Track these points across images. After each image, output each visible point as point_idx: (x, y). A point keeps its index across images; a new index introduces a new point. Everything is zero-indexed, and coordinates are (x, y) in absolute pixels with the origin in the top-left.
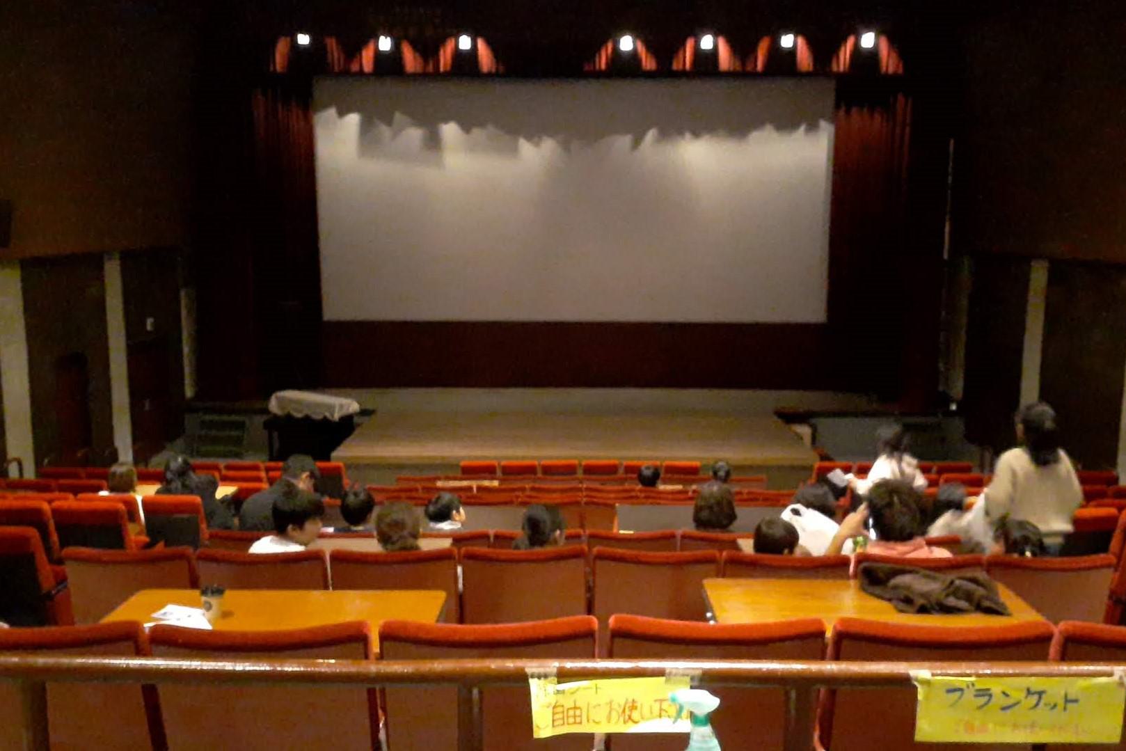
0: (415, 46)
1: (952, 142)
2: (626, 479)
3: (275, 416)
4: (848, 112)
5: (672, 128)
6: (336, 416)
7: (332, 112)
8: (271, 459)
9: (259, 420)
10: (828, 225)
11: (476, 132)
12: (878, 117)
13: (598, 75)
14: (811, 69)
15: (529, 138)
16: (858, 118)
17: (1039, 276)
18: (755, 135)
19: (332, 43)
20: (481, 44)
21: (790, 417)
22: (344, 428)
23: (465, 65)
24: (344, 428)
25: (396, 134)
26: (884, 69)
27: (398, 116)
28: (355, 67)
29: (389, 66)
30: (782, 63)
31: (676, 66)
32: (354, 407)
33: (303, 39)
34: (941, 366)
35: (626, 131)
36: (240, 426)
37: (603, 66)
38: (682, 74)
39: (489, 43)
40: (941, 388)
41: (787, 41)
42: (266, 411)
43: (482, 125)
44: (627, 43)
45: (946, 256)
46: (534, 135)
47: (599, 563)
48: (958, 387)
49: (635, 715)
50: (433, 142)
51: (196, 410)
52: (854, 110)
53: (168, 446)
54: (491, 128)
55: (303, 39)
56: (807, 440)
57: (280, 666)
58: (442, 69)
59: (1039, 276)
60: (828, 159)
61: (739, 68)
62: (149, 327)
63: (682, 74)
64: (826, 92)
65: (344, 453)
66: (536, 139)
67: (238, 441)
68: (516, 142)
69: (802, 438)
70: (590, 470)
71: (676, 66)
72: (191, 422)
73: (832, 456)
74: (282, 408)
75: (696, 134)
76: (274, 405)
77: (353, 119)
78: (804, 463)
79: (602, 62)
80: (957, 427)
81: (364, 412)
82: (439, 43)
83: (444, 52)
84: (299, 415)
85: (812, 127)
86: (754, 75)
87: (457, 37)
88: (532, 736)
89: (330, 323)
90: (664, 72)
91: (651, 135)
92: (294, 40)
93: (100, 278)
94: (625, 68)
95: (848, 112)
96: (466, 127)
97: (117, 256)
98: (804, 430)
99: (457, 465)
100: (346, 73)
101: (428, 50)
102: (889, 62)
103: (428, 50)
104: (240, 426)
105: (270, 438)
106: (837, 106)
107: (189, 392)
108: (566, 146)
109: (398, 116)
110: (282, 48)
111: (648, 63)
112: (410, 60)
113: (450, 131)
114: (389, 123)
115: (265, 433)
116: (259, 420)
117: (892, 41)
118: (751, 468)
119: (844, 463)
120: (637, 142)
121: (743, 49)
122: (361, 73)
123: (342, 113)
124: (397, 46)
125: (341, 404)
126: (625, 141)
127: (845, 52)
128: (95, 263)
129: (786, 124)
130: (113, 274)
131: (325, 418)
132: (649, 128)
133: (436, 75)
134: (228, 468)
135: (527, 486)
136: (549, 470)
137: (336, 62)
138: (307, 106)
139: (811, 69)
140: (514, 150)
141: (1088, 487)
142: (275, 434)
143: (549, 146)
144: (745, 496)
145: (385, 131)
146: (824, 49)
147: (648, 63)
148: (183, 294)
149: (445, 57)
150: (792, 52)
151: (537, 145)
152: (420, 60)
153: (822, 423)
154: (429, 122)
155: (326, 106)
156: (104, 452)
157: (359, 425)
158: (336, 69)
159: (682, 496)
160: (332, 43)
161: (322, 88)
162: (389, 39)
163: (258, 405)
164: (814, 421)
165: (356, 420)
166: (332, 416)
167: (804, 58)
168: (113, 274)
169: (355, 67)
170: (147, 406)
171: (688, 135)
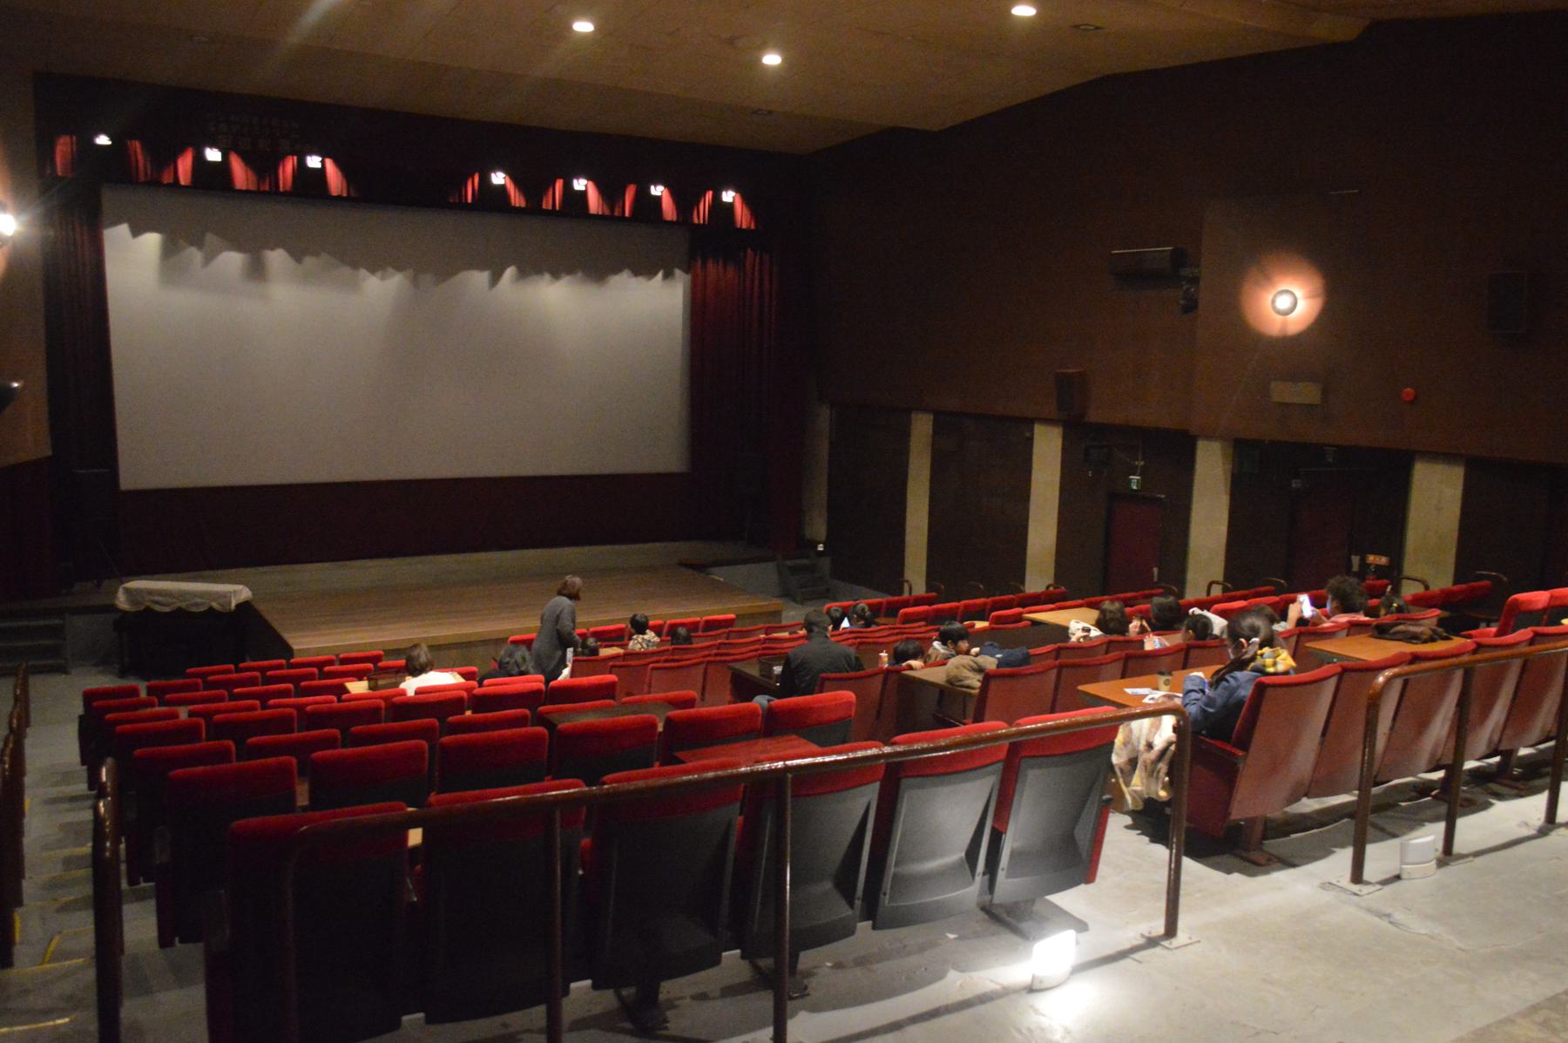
0: (248, 160)
3: (125, 613)
5: (530, 268)
7: (124, 229)
11: (309, 261)
12: (731, 269)
13: (462, 206)
14: (675, 219)
15: (373, 271)
17: (922, 428)
19: (136, 145)
20: (329, 163)
23: (212, 180)
25: (208, 259)
26: (513, 204)
27: (210, 238)
28: (167, 178)
31: (547, 204)
33: (103, 140)
35: (481, 267)
37: (469, 200)
38: (552, 213)
39: (337, 162)
41: (314, 162)
42: (112, 608)
43: (316, 254)
46: (376, 265)
49: (1269, 610)
50: (257, 270)
52: (710, 265)
54: (325, 257)
57: (593, 790)
58: (281, 189)
59: (922, 428)
60: (685, 306)
61: (607, 212)
71: (547, 204)
75: (556, 275)
77: (152, 241)
83: (284, 172)
84: (167, 609)
90: (533, 209)
91: (510, 272)
94: (494, 200)
96: (297, 255)
100: (154, 183)
102: (742, 217)
103: (263, 165)
108: (415, 281)
109: (210, 238)
111: (517, 199)
112: (241, 174)
113: (277, 258)
114: (198, 244)
119: (626, 638)
120: (496, 278)
121: (610, 193)
123: (136, 231)
126: (480, 278)
129: (644, 269)
133: (274, 193)
139: (675, 219)
141: (529, 723)
145: (195, 255)
146: (685, 202)
147: (517, 199)
150: (584, 194)
152: (253, 178)
154: (254, 248)
155: (116, 222)
158: (142, 179)
167: (594, 202)
171: (547, 276)
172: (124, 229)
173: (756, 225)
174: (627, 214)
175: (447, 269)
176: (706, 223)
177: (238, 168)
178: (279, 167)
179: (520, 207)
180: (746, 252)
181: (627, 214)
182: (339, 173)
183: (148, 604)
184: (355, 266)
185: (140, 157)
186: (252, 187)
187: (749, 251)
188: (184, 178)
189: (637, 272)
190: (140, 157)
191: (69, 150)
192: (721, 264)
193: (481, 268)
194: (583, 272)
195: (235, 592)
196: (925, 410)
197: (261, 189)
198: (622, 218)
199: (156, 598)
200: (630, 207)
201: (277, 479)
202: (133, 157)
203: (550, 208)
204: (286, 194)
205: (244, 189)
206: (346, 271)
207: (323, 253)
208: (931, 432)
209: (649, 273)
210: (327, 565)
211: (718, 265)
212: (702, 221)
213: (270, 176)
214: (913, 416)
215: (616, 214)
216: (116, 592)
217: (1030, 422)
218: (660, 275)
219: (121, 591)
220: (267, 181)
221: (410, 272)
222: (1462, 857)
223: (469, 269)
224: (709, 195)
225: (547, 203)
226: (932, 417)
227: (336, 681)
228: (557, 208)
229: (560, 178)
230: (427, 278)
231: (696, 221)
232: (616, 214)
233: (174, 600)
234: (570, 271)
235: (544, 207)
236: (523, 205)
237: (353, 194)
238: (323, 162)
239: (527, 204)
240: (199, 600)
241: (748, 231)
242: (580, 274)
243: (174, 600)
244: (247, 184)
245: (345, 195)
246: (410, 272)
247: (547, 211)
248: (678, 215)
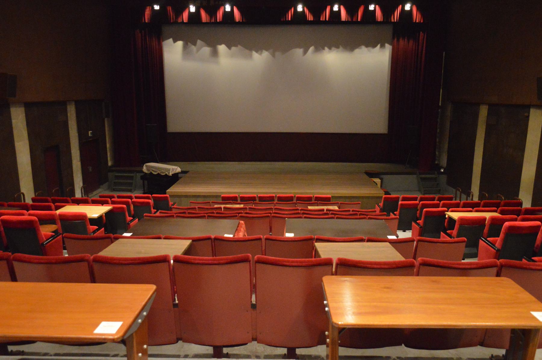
0: (206, 11)
1: (444, 53)
2: (296, 203)
3: (146, 173)
4: (398, 40)
5: (319, 48)
6: (171, 174)
7: (171, 40)
8: (144, 193)
9: (139, 175)
10: (389, 85)
11: (233, 48)
12: (411, 42)
15: (257, 52)
16: (402, 43)
17: (484, 111)
18: (357, 51)
19: (169, 8)
20: (235, 10)
21: (371, 175)
22: (174, 179)
23: (229, 17)
24: (174, 179)
25: (198, 50)
27: (199, 42)
29: (195, 19)
30: (369, 16)
32: (179, 170)
33: (157, 7)
34: (437, 153)
35: (300, 47)
36: (131, 178)
37: (290, 19)
38: (325, 23)
39: (239, 9)
40: (436, 163)
41: (372, 7)
42: (142, 172)
44: (300, 8)
45: (440, 105)
46: (259, 50)
47: (258, 265)
48: (444, 161)
50: (215, 53)
51: (113, 171)
52: (401, 40)
53: (101, 186)
54: (239, 47)
55: (157, 7)
56: (379, 185)
58: (218, 21)
59: (484, 111)
61: (350, 20)
62: (90, 135)
63: (325, 23)
64: (388, 30)
65: (174, 189)
66: (260, 52)
67: (131, 184)
68: (252, 52)
69: (377, 184)
70: (280, 199)
72: (110, 175)
73: (390, 192)
74: (148, 170)
75: (330, 48)
76: (145, 169)
77: (180, 43)
78: (378, 195)
79: (289, 17)
80: (443, 179)
81: (183, 172)
82: (218, 8)
84: (155, 173)
85: (383, 46)
86: (357, 23)
87: (224, 5)
88: (384, 134)
89: (389, 131)
90: (317, 22)
91: (312, 49)
92: (153, 8)
93: (65, 112)
94: (299, 19)
95: (398, 40)
96: (229, 47)
97: (73, 103)
98: (378, 181)
99: (220, 196)
100: (176, 23)
101: (212, 11)
102: (417, 17)
104: (131, 178)
105: (143, 182)
106: (393, 38)
107: (110, 164)
108: (273, 55)
109: (199, 42)
110: (148, 12)
111: (310, 17)
112: (204, 15)
113: (222, 48)
114: (195, 44)
115: (142, 181)
116: (139, 175)
117: (418, 9)
118: (353, 197)
120: (305, 52)
121: (351, 12)
122: (183, 23)
123: (175, 41)
124: (198, 10)
125: (173, 169)
127: (397, 13)
128: (63, 105)
129: (371, 44)
130: (72, 111)
131: (166, 174)
132: (311, 46)
133: (216, 23)
134: (119, 197)
135: (247, 207)
136: (262, 199)
137: (172, 17)
138: (160, 38)
140: (251, 56)
142: (146, 182)
143: (266, 54)
144: (351, 213)
145: (194, 48)
146: (387, 12)
147: (310, 17)
148: (106, 119)
149: (220, 15)
151: (261, 54)
152: (208, 17)
153: (385, 177)
154: (213, 45)
156: (167, 172)
157: (181, 178)
158: (172, 21)
159: (321, 213)
160: (169, 8)
161: (166, 29)
162: (194, 7)
163: (138, 169)
164: (382, 176)
165: (180, 175)
166: (169, 173)
167: (379, 14)
168: (72, 111)
169: (180, 20)
170: (90, 169)
172: (171, 40)
173: (424, 21)
174: (359, 20)
175: (286, 49)
176: (398, 21)
177: (203, 13)
178: (217, 12)
179: (311, 21)
180: (419, 34)
181: (359, 20)
182: (239, 13)
183: (151, 171)
184: (251, 49)
185: (171, 13)
186: (208, 21)
187: (421, 32)
188: (185, 19)
189: (367, 46)
190: (171, 13)
191: (149, 13)
192: (406, 40)
193: (300, 48)
194: (315, 47)
195: (173, 169)
196: (486, 104)
197: (212, 21)
198: (357, 23)
199: (153, 169)
200: (328, 16)
201: (222, 131)
202: (169, 12)
203: (324, 20)
204: (220, 23)
205: (205, 22)
206: (247, 51)
207: (239, 45)
208: (486, 114)
209: (374, 46)
210: (236, 163)
211: (404, 41)
212: (396, 21)
213: (214, 16)
214: (481, 107)
215: (354, 20)
216: (143, 166)
217: (527, 107)
218: (379, 46)
219: (145, 165)
220: (213, 18)
221: (271, 50)
222: (255, 264)
223: (296, 48)
224: (400, 8)
225: (323, 18)
226: (487, 107)
227: (223, 202)
228: (327, 20)
229: (329, 5)
230: (277, 54)
231: (393, 21)
232: (354, 20)
233: (157, 170)
234: (337, 47)
235: (321, 19)
236: (312, 20)
237: (244, 21)
238: (375, 8)
239: (314, 19)
240: (163, 171)
241: (419, 23)
242: (341, 48)
243: (157, 170)
244: (206, 19)
245: (241, 21)
246: (271, 50)
247: (323, 21)
248: (383, 19)
